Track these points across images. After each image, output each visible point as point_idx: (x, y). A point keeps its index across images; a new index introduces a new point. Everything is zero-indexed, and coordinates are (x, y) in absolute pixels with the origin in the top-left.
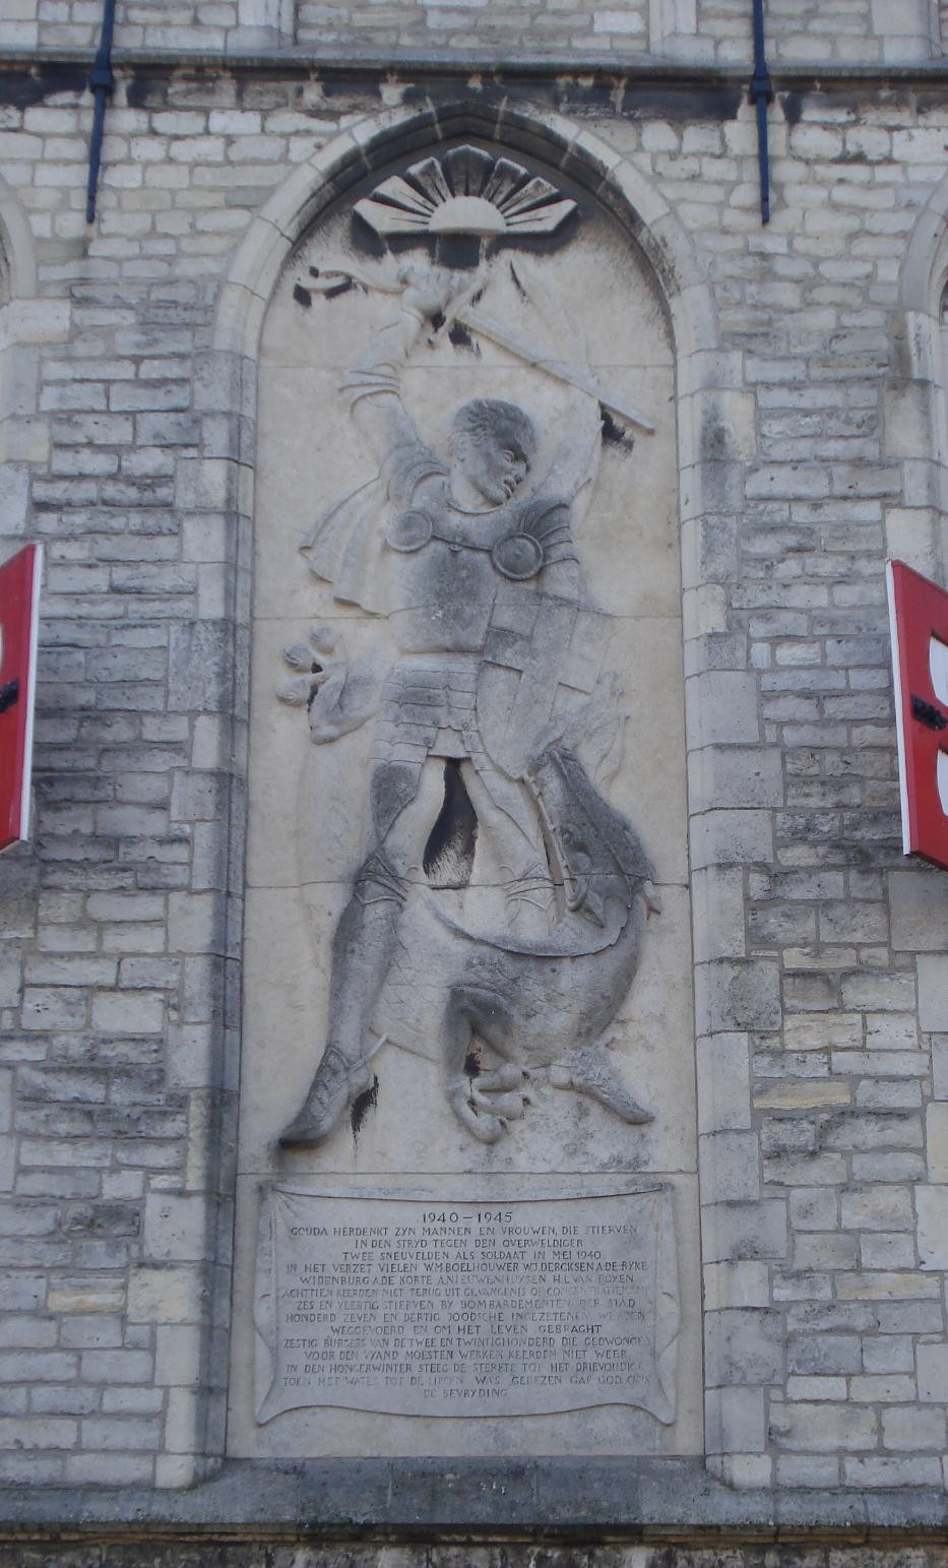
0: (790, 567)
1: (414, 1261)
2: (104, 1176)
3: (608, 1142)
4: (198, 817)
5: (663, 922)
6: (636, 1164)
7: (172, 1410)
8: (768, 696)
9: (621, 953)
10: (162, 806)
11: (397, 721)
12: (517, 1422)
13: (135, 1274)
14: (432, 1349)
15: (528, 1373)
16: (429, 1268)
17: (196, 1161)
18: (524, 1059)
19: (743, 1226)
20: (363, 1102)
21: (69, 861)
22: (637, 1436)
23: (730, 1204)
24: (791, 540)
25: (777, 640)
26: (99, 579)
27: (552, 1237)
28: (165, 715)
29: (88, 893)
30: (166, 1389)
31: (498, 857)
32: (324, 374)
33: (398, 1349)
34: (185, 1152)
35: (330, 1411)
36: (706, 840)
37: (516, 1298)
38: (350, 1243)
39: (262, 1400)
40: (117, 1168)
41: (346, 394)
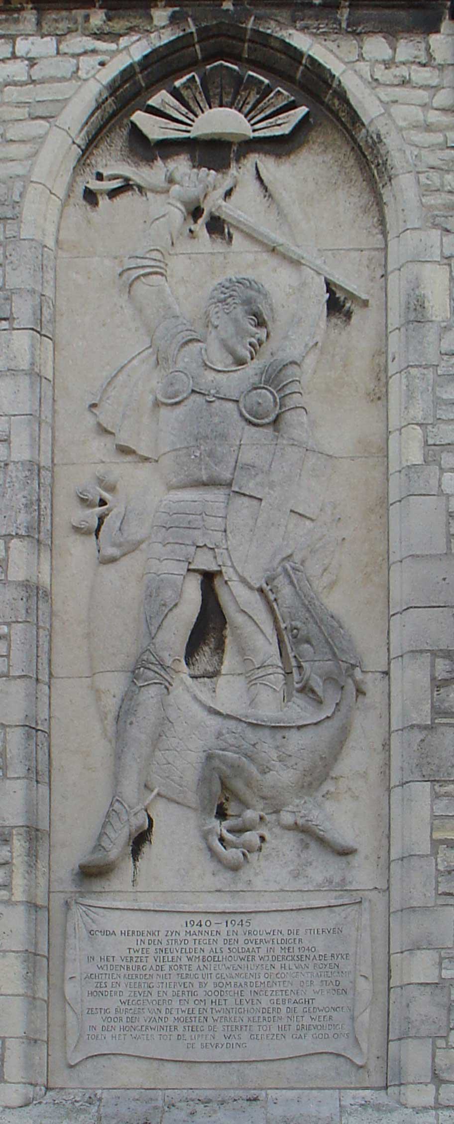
1: (179, 954)
3: (322, 868)
12: (253, 1065)
16: (190, 959)
27: (280, 937)
31: (242, 651)
32: (107, 262)
33: (169, 1015)
38: (132, 942)
41: (125, 275)
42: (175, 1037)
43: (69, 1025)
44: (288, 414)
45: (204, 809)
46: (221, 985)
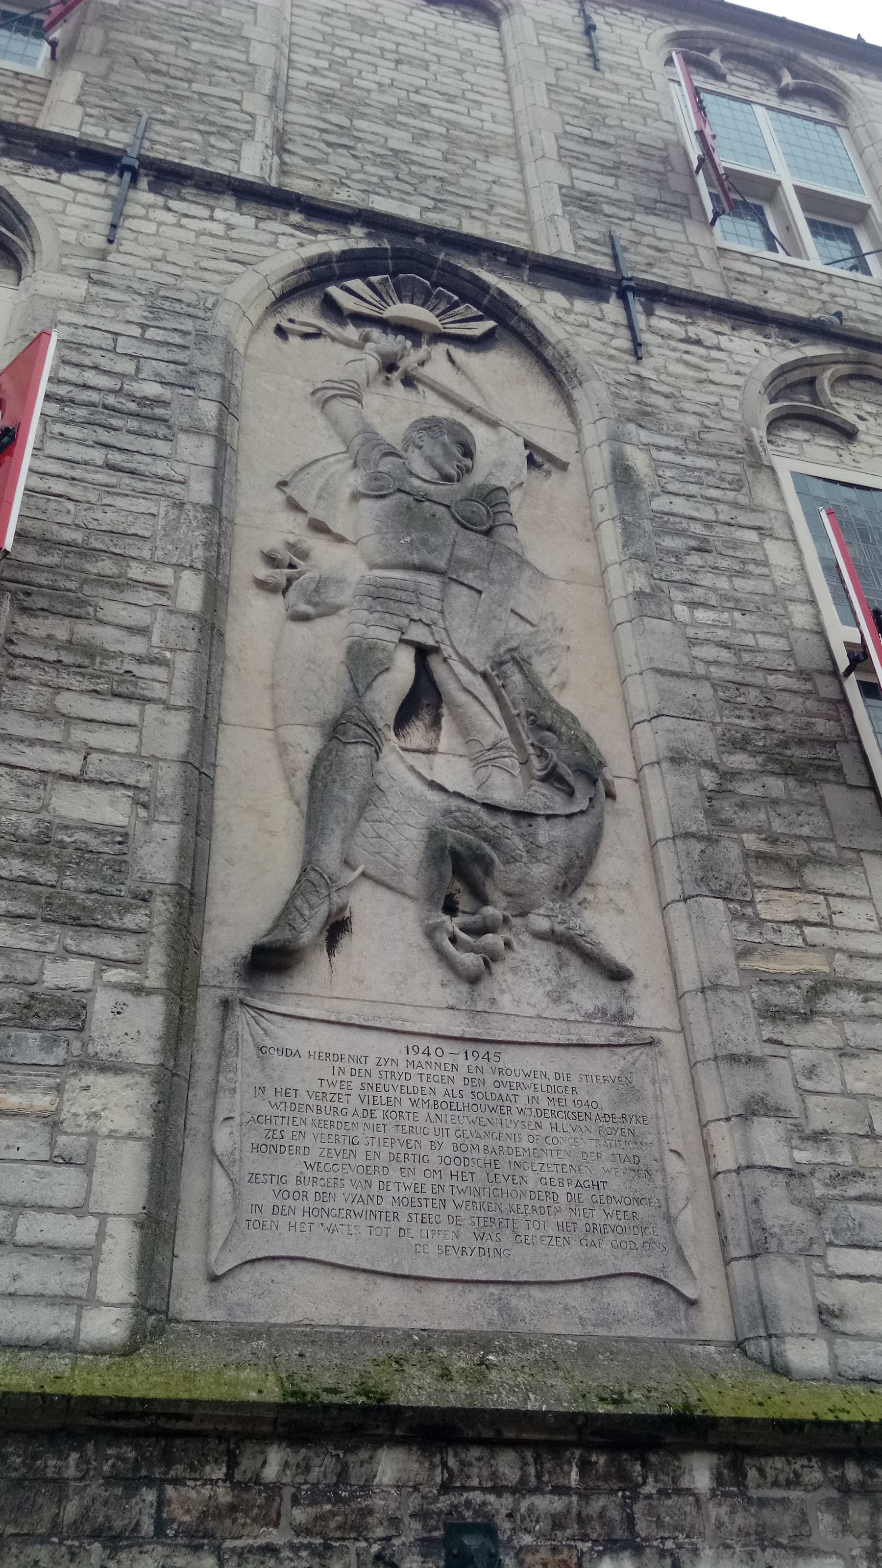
0: (695, 559)
1: (398, 1095)
2: (47, 962)
3: (591, 994)
4: (180, 646)
5: (617, 806)
6: (620, 1018)
7: (108, 1245)
8: (693, 642)
9: (582, 826)
10: (143, 631)
11: (371, 610)
12: (524, 1290)
13: (75, 1074)
14: (422, 1196)
15: (532, 1232)
16: (414, 1103)
17: (157, 958)
18: (504, 904)
19: (747, 1083)
20: (337, 929)
21: (41, 660)
22: (659, 1314)
23: (733, 1058)
24: (693, 543)
25: (694, 605)
26: (98, 456)
27: (545, 1082)
28: (153, 564)
29: (58, 689)
30: (103, 1217)
31: (465, 731)
32: (299, 382)
33: (383, 1193)
34: (144, 947)
35: (302, 1265)
36: (651, 741)
37: (513, 1145)
38: (325, 1069)
39: (220, 1244)
40: (67, 953)
41: (319, 394)
42: (394, 1232)
43: (217, 1200)
44: (502, 529)
45: (430, 899)
46: (457, 1161)
